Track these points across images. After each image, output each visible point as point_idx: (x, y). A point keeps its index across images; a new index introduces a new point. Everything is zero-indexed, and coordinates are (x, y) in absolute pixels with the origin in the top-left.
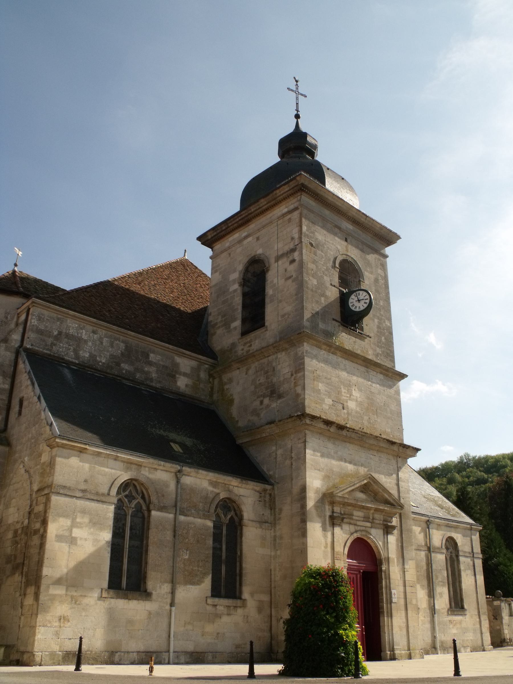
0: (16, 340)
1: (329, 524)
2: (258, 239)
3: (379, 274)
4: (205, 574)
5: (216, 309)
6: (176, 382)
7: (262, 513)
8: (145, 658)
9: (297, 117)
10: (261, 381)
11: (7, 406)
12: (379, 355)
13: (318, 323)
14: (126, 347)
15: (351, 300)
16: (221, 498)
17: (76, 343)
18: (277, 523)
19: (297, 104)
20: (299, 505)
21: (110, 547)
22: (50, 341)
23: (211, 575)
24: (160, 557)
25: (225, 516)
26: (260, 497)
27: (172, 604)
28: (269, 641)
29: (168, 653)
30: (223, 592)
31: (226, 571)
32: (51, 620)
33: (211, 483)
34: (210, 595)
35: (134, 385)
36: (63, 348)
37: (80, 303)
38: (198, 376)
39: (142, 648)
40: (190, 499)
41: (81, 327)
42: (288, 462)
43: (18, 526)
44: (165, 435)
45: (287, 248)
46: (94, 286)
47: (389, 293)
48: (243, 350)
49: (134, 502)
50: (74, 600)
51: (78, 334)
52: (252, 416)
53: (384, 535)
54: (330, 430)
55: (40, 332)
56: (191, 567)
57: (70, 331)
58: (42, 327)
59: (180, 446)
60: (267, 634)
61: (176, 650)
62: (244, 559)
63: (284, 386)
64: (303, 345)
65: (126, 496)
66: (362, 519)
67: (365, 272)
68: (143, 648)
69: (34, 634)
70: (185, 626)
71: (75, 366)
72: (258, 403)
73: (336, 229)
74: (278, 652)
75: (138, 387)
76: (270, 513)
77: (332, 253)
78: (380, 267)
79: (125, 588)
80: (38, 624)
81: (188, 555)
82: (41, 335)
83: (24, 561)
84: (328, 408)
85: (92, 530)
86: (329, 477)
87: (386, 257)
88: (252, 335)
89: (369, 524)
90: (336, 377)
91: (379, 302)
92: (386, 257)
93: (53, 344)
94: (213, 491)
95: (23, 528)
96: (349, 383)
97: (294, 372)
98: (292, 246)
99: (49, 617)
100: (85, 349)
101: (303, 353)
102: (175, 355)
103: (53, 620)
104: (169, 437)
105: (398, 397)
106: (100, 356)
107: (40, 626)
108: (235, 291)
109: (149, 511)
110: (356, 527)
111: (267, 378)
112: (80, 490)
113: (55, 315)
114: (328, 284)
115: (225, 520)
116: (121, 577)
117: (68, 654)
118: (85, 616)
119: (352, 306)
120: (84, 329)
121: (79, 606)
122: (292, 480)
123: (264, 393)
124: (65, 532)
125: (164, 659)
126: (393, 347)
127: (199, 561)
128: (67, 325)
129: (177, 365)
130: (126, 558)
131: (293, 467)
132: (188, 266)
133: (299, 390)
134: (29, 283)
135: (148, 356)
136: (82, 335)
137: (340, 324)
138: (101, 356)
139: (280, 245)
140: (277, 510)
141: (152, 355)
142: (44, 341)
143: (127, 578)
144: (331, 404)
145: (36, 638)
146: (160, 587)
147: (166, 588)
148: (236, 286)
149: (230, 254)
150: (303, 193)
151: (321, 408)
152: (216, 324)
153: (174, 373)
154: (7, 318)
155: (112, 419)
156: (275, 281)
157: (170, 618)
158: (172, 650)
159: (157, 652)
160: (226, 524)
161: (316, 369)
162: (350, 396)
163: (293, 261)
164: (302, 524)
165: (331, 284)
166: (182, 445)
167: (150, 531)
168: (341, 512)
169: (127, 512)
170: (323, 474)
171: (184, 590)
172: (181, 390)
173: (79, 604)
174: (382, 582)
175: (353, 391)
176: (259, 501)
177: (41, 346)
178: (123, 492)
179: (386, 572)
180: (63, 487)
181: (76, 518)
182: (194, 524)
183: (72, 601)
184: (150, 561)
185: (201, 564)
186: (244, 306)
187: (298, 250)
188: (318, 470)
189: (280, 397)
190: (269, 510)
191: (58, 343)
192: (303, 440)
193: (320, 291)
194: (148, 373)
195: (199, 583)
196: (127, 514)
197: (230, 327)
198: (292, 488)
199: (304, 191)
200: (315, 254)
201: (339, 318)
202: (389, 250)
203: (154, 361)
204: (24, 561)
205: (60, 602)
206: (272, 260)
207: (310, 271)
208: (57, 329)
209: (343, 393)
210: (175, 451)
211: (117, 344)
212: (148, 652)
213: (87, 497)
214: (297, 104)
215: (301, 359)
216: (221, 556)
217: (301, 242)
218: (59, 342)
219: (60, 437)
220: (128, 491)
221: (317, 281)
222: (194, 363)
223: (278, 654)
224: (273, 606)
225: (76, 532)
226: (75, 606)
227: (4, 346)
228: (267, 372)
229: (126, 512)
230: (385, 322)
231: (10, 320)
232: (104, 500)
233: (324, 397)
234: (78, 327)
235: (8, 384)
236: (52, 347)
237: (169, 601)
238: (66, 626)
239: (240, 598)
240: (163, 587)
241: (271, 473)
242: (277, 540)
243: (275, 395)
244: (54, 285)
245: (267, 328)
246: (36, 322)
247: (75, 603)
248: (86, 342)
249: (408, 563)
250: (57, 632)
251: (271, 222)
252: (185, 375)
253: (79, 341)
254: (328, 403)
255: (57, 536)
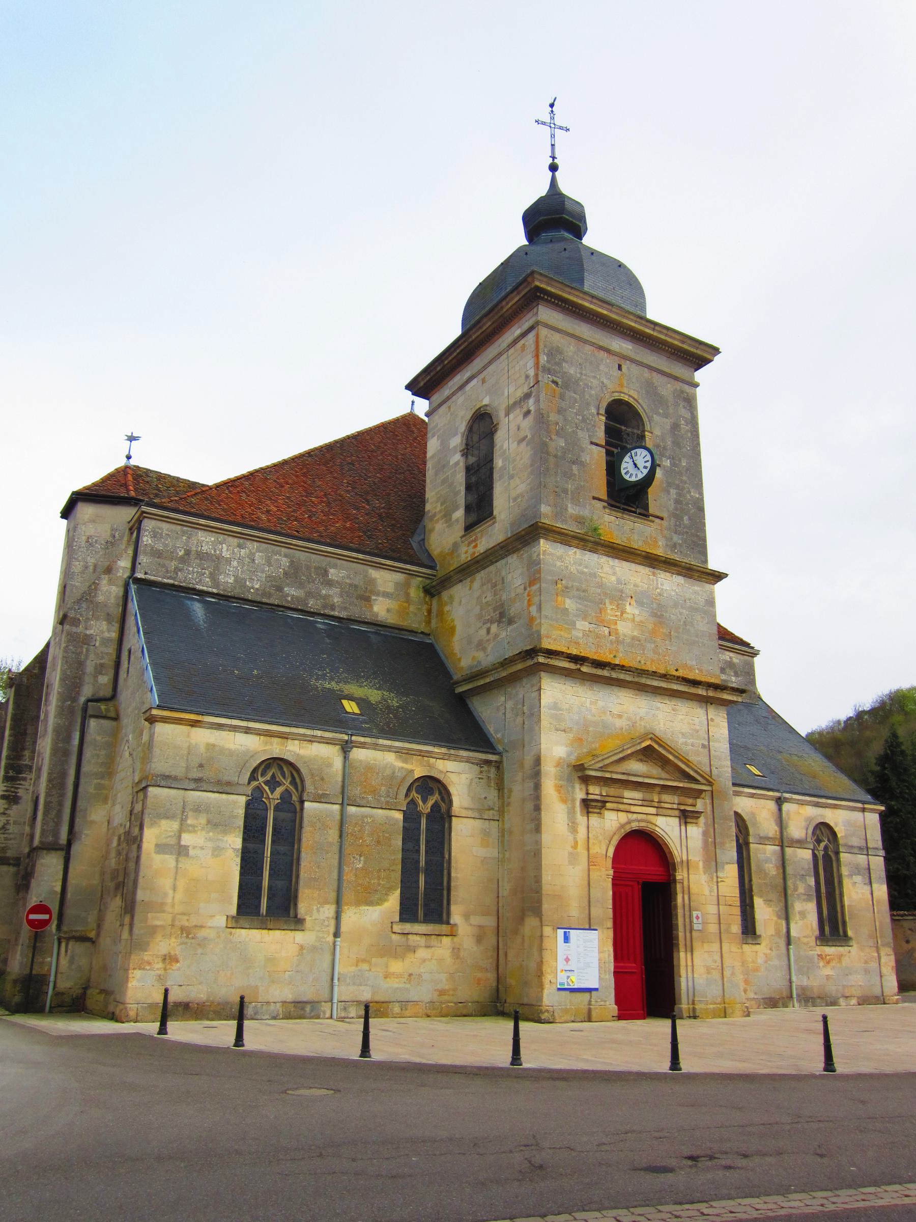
0: (124, 568)
1: (581, 811)
2: (484, 381)
3: (681, 416)
4: (390, 889)
5: (434, 493)
6: (371, 606)
7: (484, 796)
8: (294, 1011)
9: (553, 168)
10: (488, 599)
11: (115, 662)
12: (678, 546)
13: (567, 506)
14: (292, 562)
15: (623, 465)
16: (416, 777)
17: (213, 564)
18: (506, 810)
19: (553, 145)
20: (532, 784)
21: (240, 856)
22: (173, 564)
23: (399, 891)
24: (318, 867)
25: (425, 801)
26: (481, 772)
27: (336, 934)
28: (494, 984)
29: (330, 1003)
30: (421, 913)
31: (426, 882)
32: (151, 961)
33: (400, 756)
34: (397, 919)
35: (304, 617)
36: (194, 573)
37: (220, 505)
38: (407, 594)
39: (290, 997)
40: (365, 781)
41: (220, 540)
42: (519, 720)
43: (122, 831)
44: (338, 688)
45: (519, 394)
46: (247, 476)
47: (699, 445)
48: (466, 552)
49: (279, 790)
50: (184, 932)
51: (215, 551)
52: (477, 651)
53: (680, 826)
54: (582, 669)
55: (157, 554)
56: (368, 880)
57: (203, 548)
58: (160, 547)
59: (358, 704)
60: (491, 976)
61: (343, 999)
62: (453, 864)
63: (516, 605)
64: (539, 543)
65: (266, 783)
66: (640, 803)
67: (655, 416)
68: (290, 996)
69: (127, 980)
70: (357, 965)
71: (214, 598)
72: (483, 632)
73: (602, 352)
74: (505, 1002)
75: (312, 619)
76: (496, 795)
77: (593, 392)
78: (682, 404)
79: (265, 914)
80: (131, 966)
81: (362, 862)
82: (159, 557)
83: (124, 879)
84: (580, 635)
85: (211, 834)
86: (581, 740)
87: (696, 385)
88: (478, 530)
89: (653, 810)
90: (597, 587)
91: (680, 461)
92: (696, 385)
93: (177, 570)
94: (402, 768)
95: (125, 833)
96: (620, 594)
97: (528, 584)
98: (526, 389)
99: (147, 956)
100: (227, 571)
101: (539, 555)
102: (369, 567)
103: (153, 960)
104: (343, 691)
105: (711, 609)
106: (251, 579)
107: (134, 969)
108: (457, 464)
109: (302, 802)
110: (630, 815)
111: (495, 594)
112: (193, 779)
113: (179, 527)
114: (585, 443)
115: (425, 808)
116: (259, 898)
117: (177, 1006)
118: (202, 954)
119: (625, 474)
120: (225, 544)
121: (193, 941)
122: (524, 746)
123: (491, 617)
124: (169, 839)
125: (324, 1013)
126: (704, 531)
127: (380, 870)
128: (198, 540)
129: (372, 582)
130: (266, 871)
131: (526, 726)
132: (415, 426)
133: (533, 610)
134: (148, 482)
135: (326, 573)
136: (222, 552)
137: (606, 504)
138: (253, 580)
139: (512, 390)
140: (506, 791)
141: (332, 571)
142: (164, 566)
143: (269, 898)
144: (587, 629)
145: (130, 985)
146: (318, 911)
147: (329, 911)
148: (457, 457)
149: (449, 407)
150: (541, 302)
151: (570, 636)
152: (434, 515)
153: (367, 594)
154: (114, 536)
155: (255, 672)
156: (506, 446)
157: (334, 954)
158: (335, 1000)
159: (314, 1002)
160: (425, 815)
161: (560, 577)
162: (622, 613)
163: (528, 412)
164: (536, 813)
165: (592, 443)
166: (360, 702)
167: (304, 830)
168: (601, 793)
169: (268, 804)
170: (572, 735)
171: (355, 913)
172: (379, 618)
173: (193, 938)
174: (675, 899)
175: (628, 607)
176: (479, 778)
177: (160, 574)
178: (261, 776)
179: (683, 883)
180: (164, 777)
181: (186, 819)
182: (371, 816)
183: (182, 934)
184: (303, 875)
185: (383, 874)
186: (468, 488)
187: (533, 394)
188: (562, 731)
189: (511, 622)
190: (496, 791)
191: (185, 567)
192: (536, 688)
193: (570, 456)
194: (326, 597)
195: (380, 902)
196: (269, 808)
197: (450, 519)
198: (524, 759)
199: (543, 299)
200: (562, 397)
201: (603, 495)
202: (700, 375)
203: (336, 579)
204: (124, 879)
205: (163, 936)
206: (502, 414)
207: (553, 427)
208: (183, 547)
209: (608, 611)
210: (347, 713)
211: (277, 560)
212: (298, 1002)
213: (202, 789)
214: (553, 145)
215: (536, 565)
216: (418, 862)
217: (537, 382)
218: (188, 566)
219: (159, 707)
220: (270, 774)
221: (566, 440)
222: (399, 577)
223: (505, 1005)
224: (500, 934)
225: (187, 839)
226: (187, 940)
227: (107, 579)
228: (494, 586)
229: (266, 804)
230: (689, 492)
231: (118, 539)
232: (229, 791)
233: (574, 619)
234: (214, 540)
235: (114, 632)
236: (177, 574)
237: (332, 929)
238: (173, 968)
239: (448, 923)
240: (321, 909)
241: (499, 736)
242: (506, 836)
243: (504, 620)
244: (189, 481)
245: (495, 518)
246: (149, 540)
247: (187, 937)
248: (228, 561)
249: (723, 868)
250: (160, 976)
251: (500, 354)
252: (386, 595)
253: (217, 561)
254: (581, 628)
255: (157, 845)
